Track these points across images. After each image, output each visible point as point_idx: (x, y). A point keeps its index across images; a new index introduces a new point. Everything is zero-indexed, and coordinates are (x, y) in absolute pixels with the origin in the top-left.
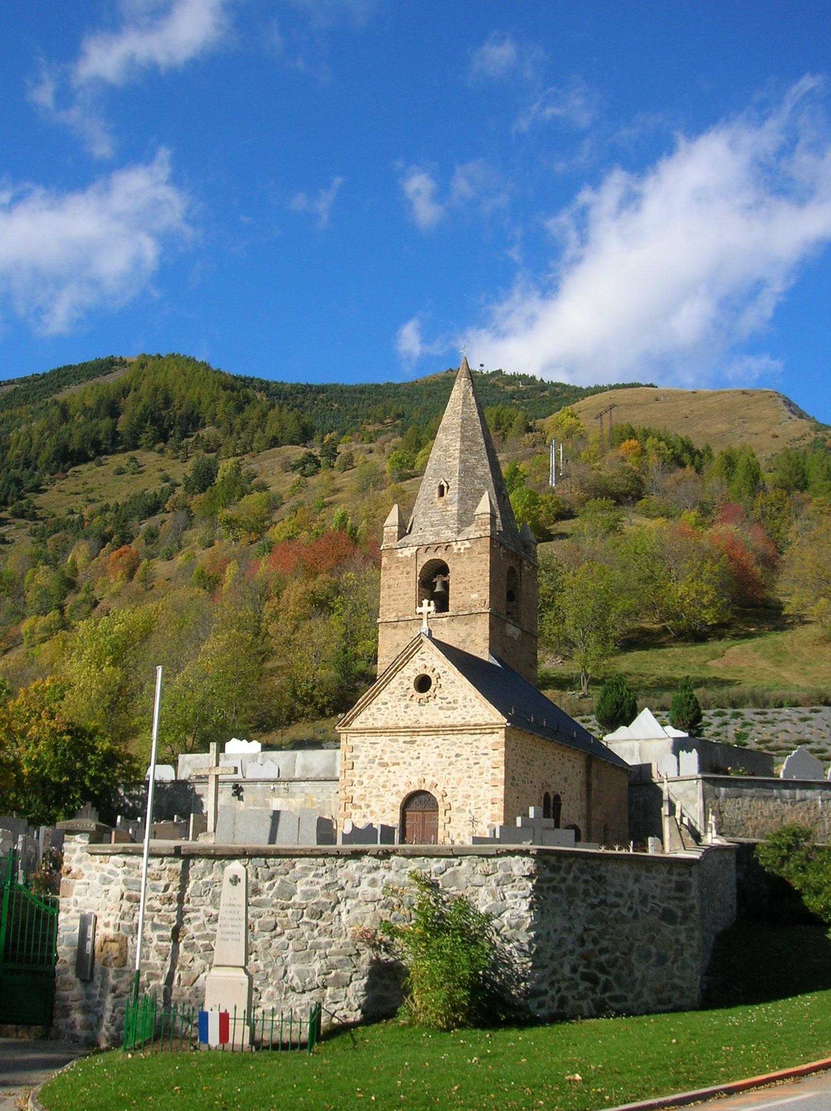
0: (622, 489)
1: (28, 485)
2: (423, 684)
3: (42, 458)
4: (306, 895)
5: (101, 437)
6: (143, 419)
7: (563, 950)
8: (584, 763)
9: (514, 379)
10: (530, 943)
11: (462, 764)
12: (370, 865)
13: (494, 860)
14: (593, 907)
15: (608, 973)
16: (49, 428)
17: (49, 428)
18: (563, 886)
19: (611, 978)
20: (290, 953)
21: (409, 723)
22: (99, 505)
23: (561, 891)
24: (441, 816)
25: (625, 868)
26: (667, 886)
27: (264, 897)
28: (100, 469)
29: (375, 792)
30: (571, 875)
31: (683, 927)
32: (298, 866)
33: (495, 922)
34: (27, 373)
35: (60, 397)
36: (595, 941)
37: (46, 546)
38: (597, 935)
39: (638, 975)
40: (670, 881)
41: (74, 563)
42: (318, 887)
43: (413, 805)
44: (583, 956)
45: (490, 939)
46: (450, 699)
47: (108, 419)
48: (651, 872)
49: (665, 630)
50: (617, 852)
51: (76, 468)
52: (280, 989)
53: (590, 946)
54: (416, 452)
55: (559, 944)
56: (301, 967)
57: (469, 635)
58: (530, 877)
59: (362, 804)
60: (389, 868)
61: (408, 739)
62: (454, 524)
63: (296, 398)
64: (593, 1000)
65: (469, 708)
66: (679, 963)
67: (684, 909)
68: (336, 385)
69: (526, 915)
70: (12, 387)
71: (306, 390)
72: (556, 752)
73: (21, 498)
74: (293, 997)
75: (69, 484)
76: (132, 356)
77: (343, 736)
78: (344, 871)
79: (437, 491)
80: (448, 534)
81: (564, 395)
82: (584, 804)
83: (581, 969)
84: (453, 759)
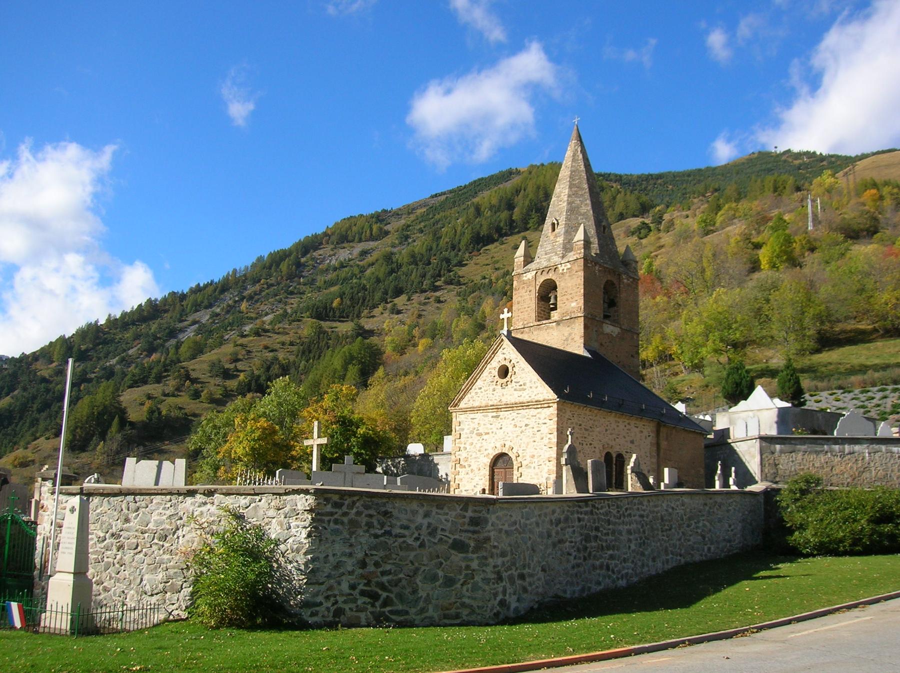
0: (862, 227)
1: (454, 262)
2: (504, 372)
3: (463, 243)
4: (158, 523)
5: (502, 225)
6: (530, 209)
7: (342, 570)
8: (654, 429)
9: (800, 155)
10: (306, 564)
11: (529, 432)
12: (200, 501)
13: (285, 497)
14: (376, 536)
15: (390, 591)
16: (468, 222)
17: (468, 222)
18: (346, 520)
19: (392, 596)
20: (145, 566)
21: (495, 403)
22: (502, 271)
23: (342, 523)
24: (515, 472)
25: (414, 505)
26: (461, 521)
27: (132, 524)
28: (502, 246)
29: (474, 455)
30: (355, 510)
31: (475, 556)
32: (154, 501)
33: (282, 547)
34: (453, 186)
35: (476, 200)
36: (377, 564)
37: (467, 302)
38: (380, 560)
39: (422, 594)
40: (464, 517)
41: (484, 312)
42: (165, 517)
43: (500, 464)
44: (362, 576)
45: (278, 560)
46: (521, 383)
47: (506, 211)
48: (442, 509)
49: (875, 330)
50: (417, 492)
51: (486, 248)
52: (137, 592)
53: (371, 568)
54: (716, 214)
55: (337, 566)
56: (151, 576)
57: (570, 334)
58: (310, 511)
59: (466, 464)
60: (213, 503)
61: (494, 414)
62: (560, 251)
63: (641, 184)
64: (372, 613)
65: (534, 389)
66: (470, 586)
67: (477, 540)
68: (669, 172)
69: (305, 541)
70: (443, 197)
71: (649, 178)
72: (621, 420)
73: (450, 271)
74: (146, 598)
75: (482, 259)
76: (523, 167)
77: (454, 414)
78: (183, 505)
79: (550, 228)
80: (556, 259)
81: (839, 163)
82: (655, 460)
83: (361, 587)
84: (524, 428)
